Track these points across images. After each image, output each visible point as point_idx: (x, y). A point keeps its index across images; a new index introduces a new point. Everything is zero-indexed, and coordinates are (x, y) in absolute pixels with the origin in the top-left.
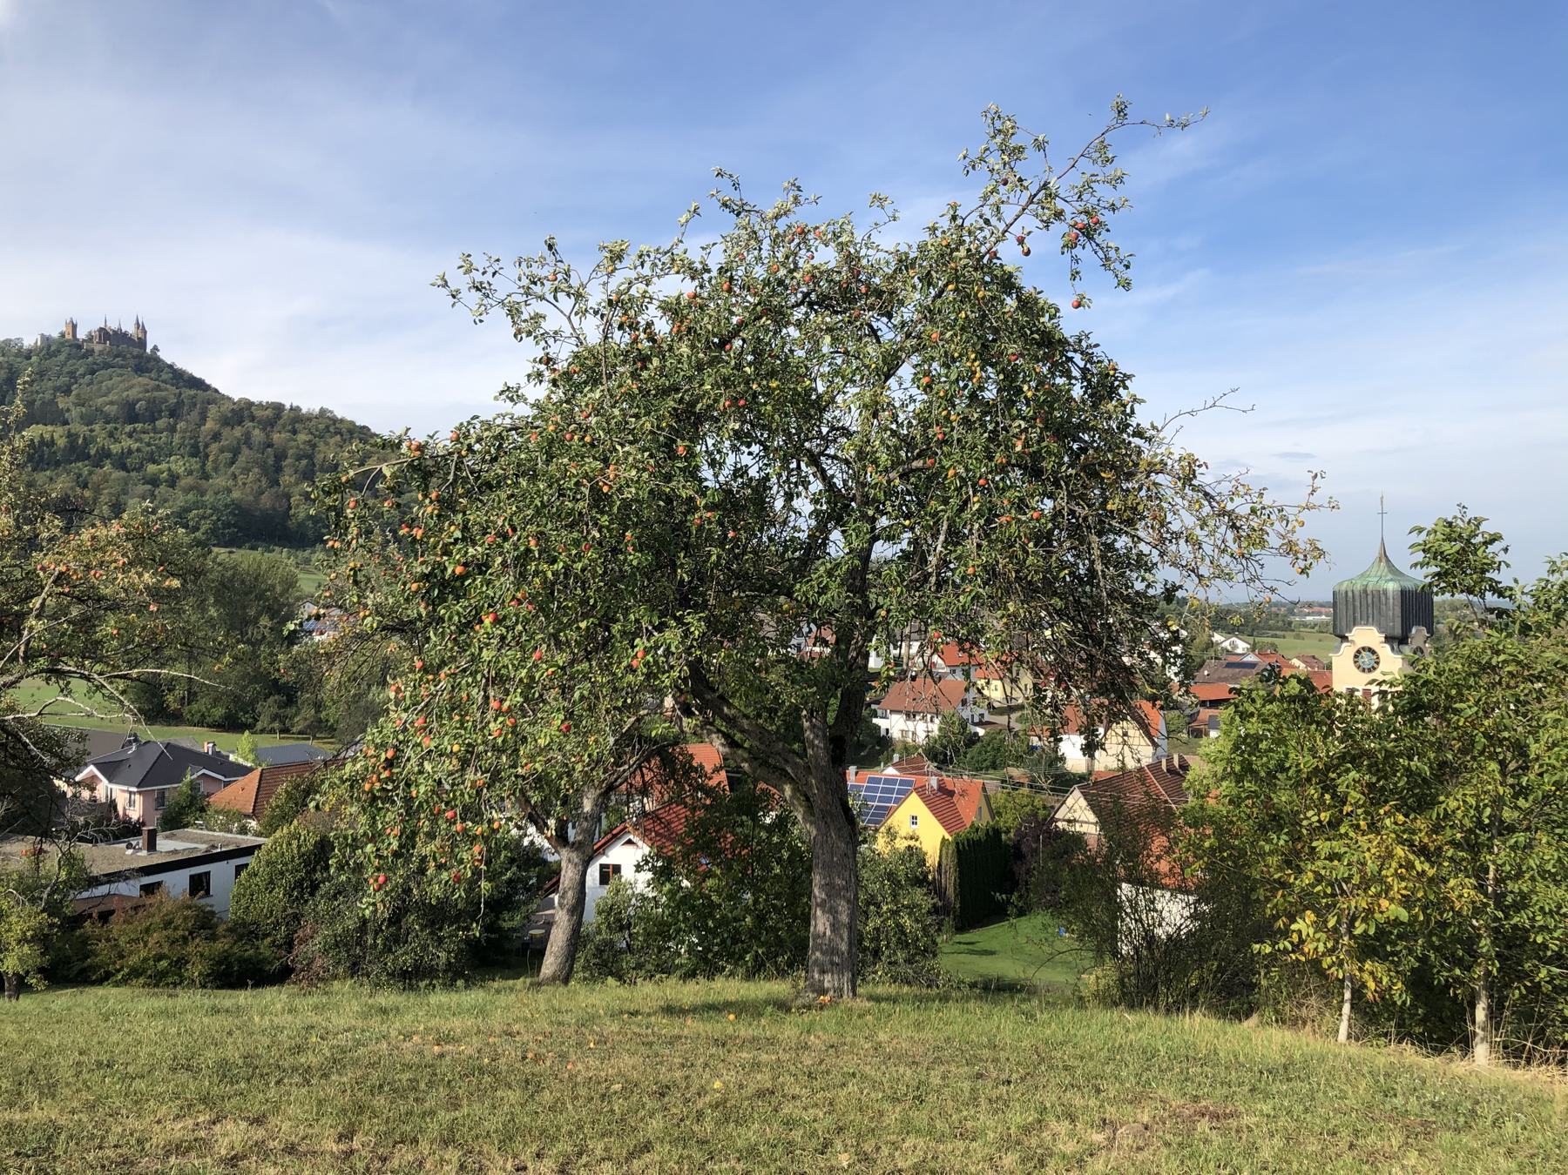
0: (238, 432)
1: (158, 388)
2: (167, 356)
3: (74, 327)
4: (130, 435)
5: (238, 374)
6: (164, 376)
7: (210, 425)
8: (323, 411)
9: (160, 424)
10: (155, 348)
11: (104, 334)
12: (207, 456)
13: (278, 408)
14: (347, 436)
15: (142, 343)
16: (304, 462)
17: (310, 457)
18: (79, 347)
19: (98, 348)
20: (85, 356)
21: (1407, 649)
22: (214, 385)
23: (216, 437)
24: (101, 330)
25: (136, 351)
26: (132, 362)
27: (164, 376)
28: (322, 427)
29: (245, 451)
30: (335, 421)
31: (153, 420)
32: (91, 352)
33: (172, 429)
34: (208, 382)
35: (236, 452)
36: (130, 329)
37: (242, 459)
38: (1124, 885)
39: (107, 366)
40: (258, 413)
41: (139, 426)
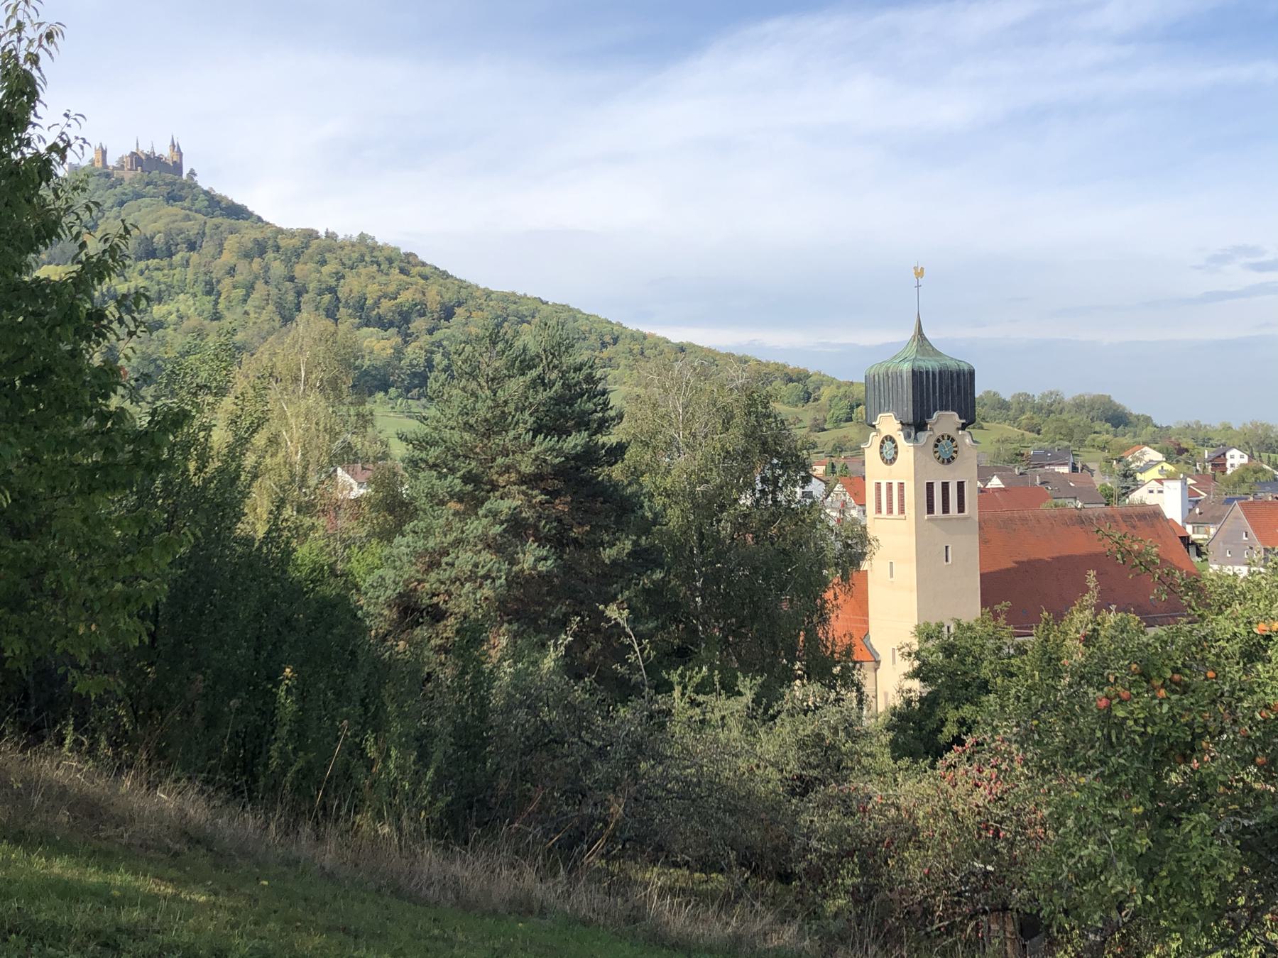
0: (257, 264)
1: (187, 218)
2: (204, 183)
3: (104, 153)
4: (142, 273)
5: (280, 203)
6: (198, 205)
7: (227, 258)
8: (363, 237)
9: (177, 258)
10: (192, 173)
11: (137, 160)
12: (219, 294)
13: (311, 235)
14: (384, 266)
15: (178, 167)
16: (327, 297)
17: (332, 290)
18: (108, 176)
19: (128, 175)
20: (113, 186)
21: (923, 436)
22: (257, 213)
23: (231, 271)
24: (133, 154)
25: (169, 177)
26: (165, 190)
27: (198, 205)
28: (355, 256)
29: (259, 285)
30: (374, 248)
31: (171, 255)
32: (120, 181)
33: (187, 264)
34: (250, 209)
35: (250, 288)
36: (164, 151)
37: (255, 295)
38: (1235, 452)
39: (138, 196)
40: (282, 243)
41: (153, 262)
